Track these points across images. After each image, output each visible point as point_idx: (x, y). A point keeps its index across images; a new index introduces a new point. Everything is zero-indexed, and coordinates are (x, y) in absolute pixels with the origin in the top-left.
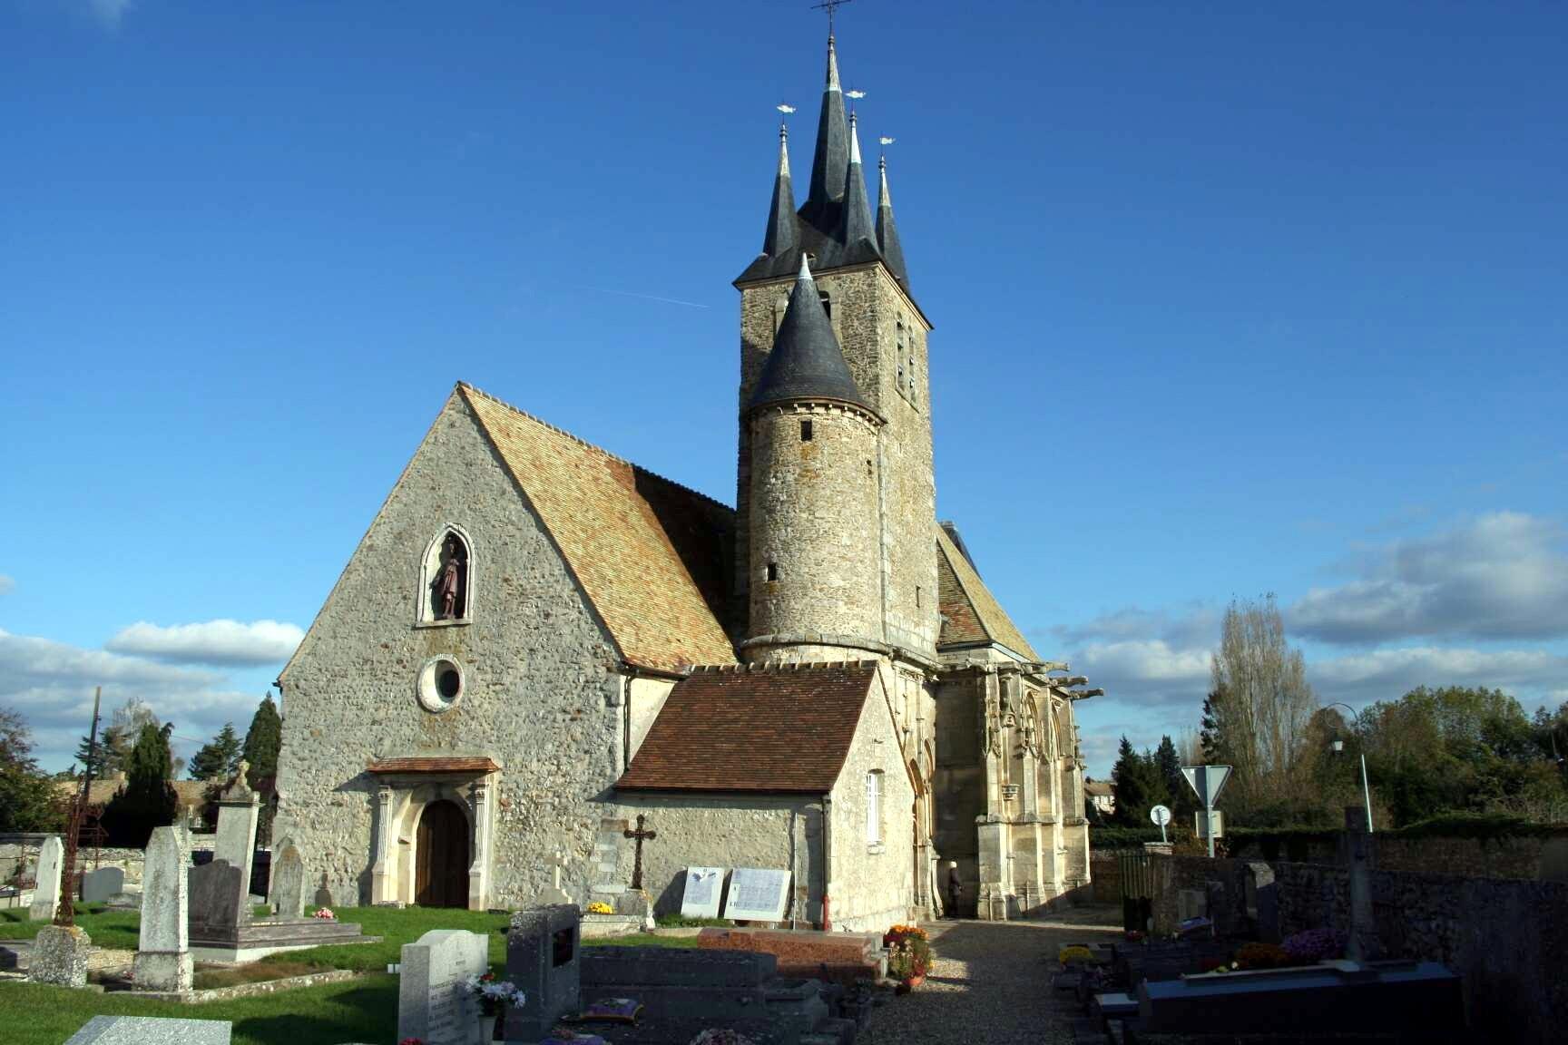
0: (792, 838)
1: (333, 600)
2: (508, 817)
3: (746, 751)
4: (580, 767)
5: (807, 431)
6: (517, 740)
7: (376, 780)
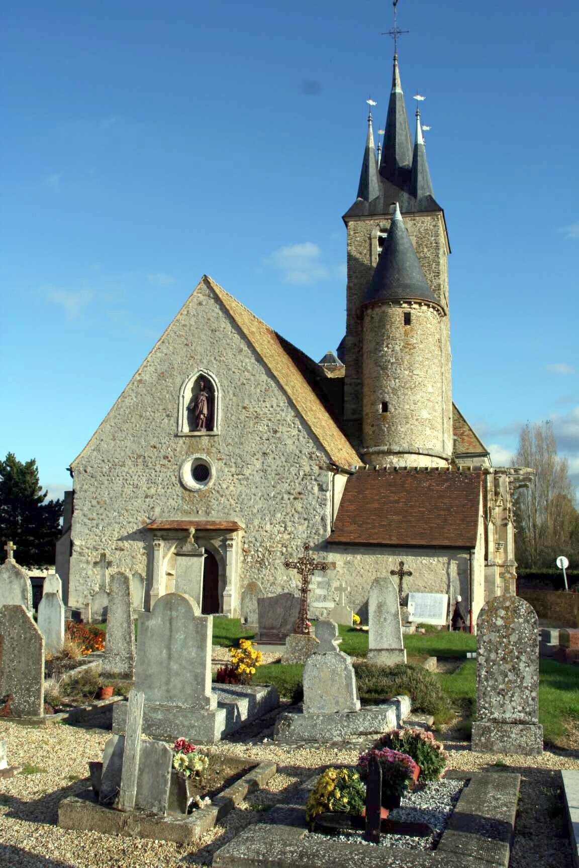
0: (448, 574)
1: (112, 414)
2: (249, 559)
3: (410, 521)
4: (301, 529)
5: (408, 319)
6: (255, 511)
7: (150, 534)
